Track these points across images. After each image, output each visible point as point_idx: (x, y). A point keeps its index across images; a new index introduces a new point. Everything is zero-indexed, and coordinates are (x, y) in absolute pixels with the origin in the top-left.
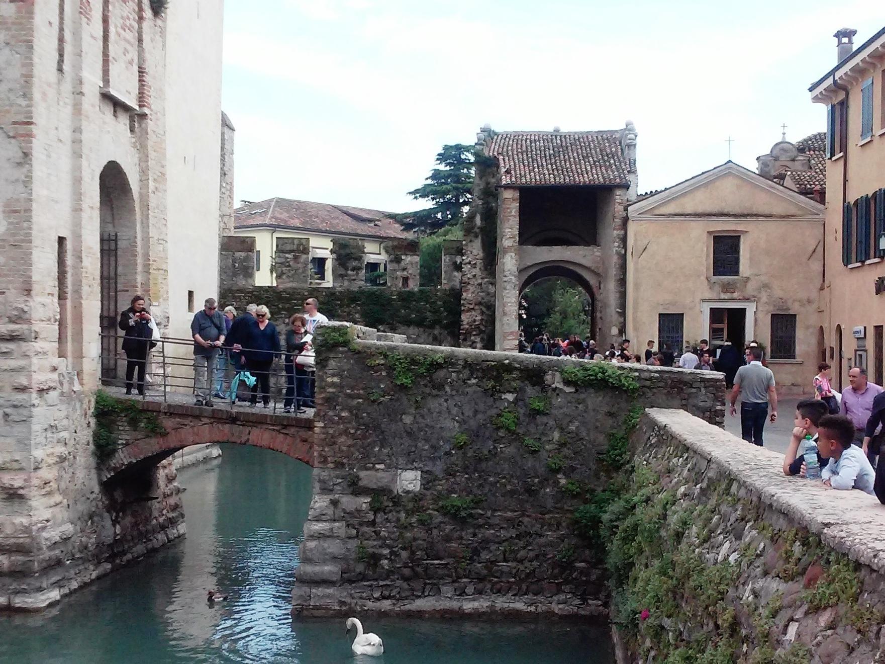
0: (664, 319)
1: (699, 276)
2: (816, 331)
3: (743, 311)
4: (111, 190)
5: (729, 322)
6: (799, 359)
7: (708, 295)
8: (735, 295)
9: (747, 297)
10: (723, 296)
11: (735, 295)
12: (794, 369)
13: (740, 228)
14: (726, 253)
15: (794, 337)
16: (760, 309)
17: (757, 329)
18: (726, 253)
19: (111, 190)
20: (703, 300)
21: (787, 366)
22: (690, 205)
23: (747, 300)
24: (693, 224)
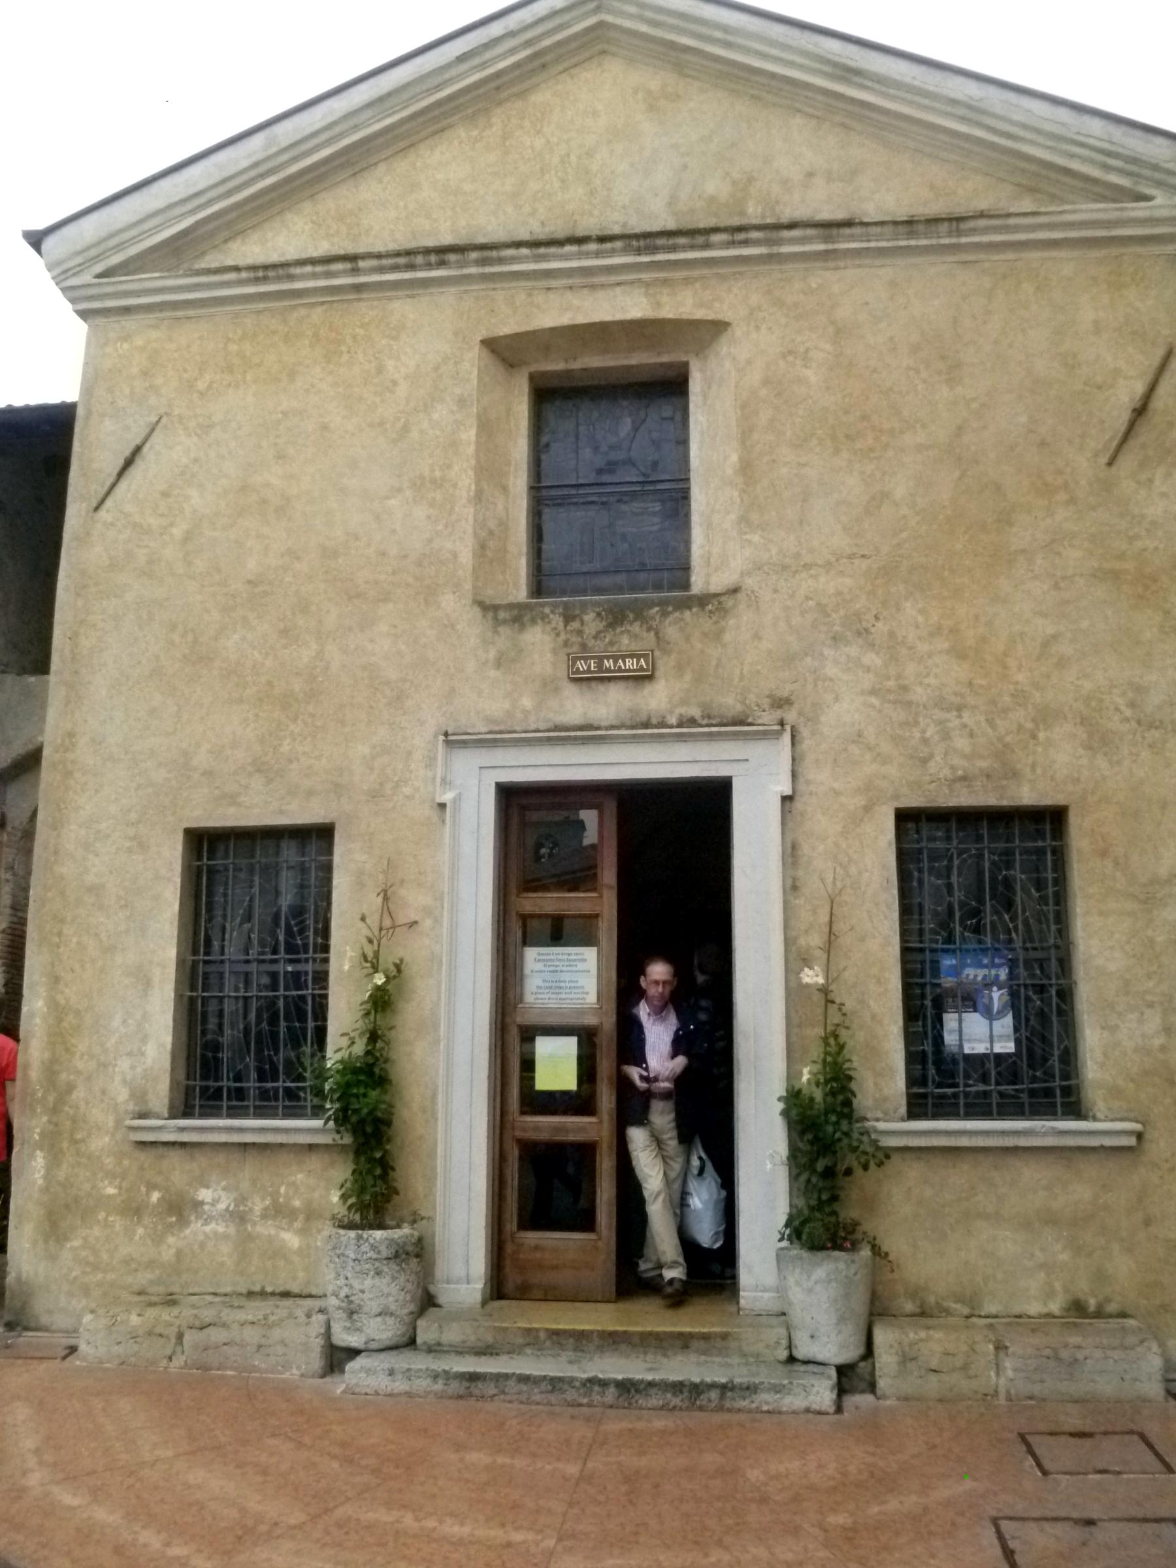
0: (218, 858)
1: (429, 594)
2: (144, 1157)
3: (708, 803)
4: (383, 1327)
5: (647, 869)
6: (1103, 1125)
7: (487, 701)
8: (657, 698)
9: (730, 703)
10: (576, 706)
11: (657, 698)
12: (1079, 1191)
13: (681, 304)
14: (602, 427)
15: (1065, 964)
16: (819, 777)
17: (810, 920)
18: (602, 427)
19: (383, 1327)
20: (454, 741)
21: (1031, 1173)
22: (388, 209)
23: (736, 725)
24: (403, 309)
